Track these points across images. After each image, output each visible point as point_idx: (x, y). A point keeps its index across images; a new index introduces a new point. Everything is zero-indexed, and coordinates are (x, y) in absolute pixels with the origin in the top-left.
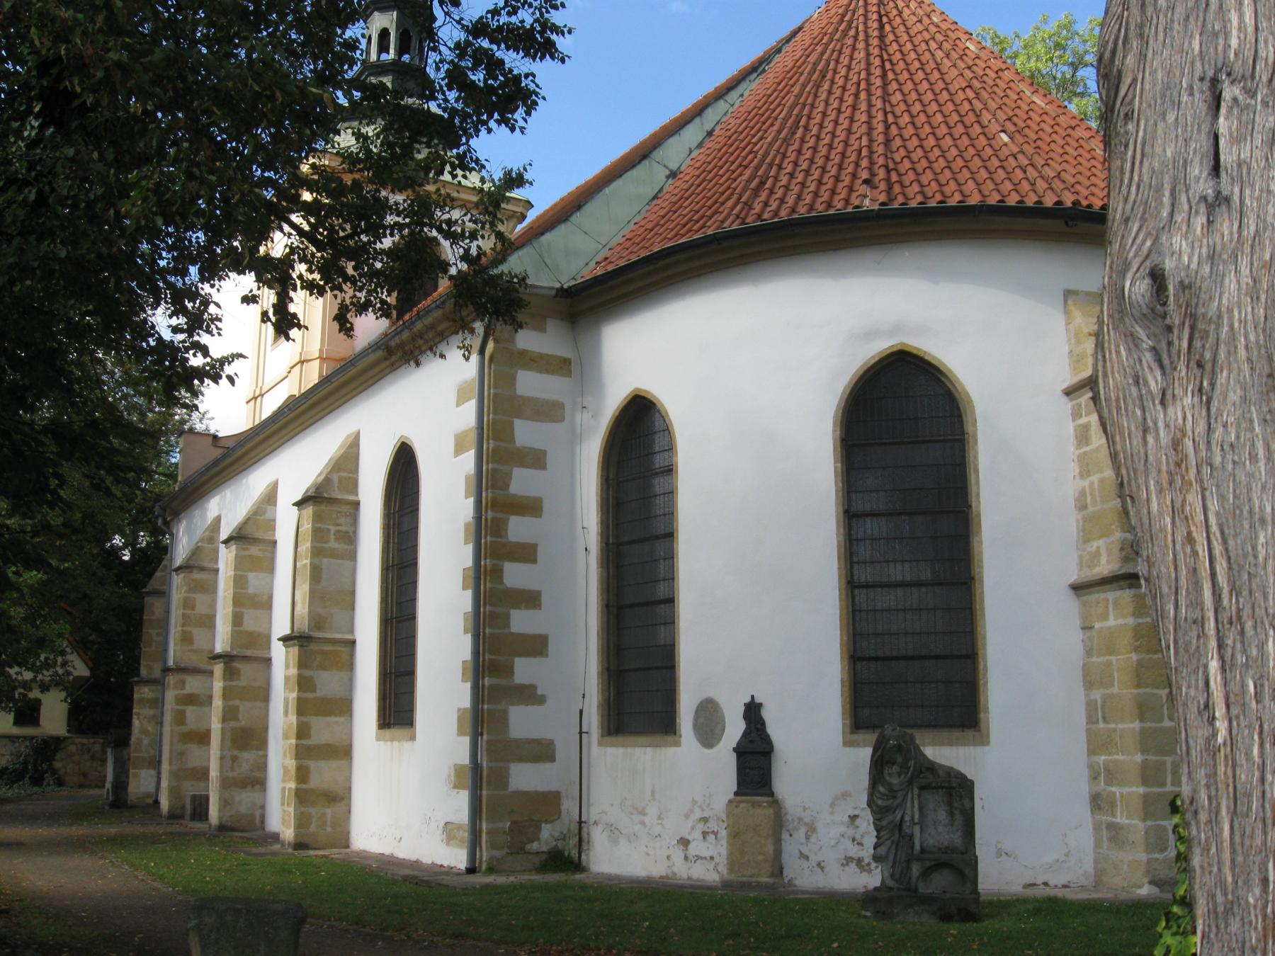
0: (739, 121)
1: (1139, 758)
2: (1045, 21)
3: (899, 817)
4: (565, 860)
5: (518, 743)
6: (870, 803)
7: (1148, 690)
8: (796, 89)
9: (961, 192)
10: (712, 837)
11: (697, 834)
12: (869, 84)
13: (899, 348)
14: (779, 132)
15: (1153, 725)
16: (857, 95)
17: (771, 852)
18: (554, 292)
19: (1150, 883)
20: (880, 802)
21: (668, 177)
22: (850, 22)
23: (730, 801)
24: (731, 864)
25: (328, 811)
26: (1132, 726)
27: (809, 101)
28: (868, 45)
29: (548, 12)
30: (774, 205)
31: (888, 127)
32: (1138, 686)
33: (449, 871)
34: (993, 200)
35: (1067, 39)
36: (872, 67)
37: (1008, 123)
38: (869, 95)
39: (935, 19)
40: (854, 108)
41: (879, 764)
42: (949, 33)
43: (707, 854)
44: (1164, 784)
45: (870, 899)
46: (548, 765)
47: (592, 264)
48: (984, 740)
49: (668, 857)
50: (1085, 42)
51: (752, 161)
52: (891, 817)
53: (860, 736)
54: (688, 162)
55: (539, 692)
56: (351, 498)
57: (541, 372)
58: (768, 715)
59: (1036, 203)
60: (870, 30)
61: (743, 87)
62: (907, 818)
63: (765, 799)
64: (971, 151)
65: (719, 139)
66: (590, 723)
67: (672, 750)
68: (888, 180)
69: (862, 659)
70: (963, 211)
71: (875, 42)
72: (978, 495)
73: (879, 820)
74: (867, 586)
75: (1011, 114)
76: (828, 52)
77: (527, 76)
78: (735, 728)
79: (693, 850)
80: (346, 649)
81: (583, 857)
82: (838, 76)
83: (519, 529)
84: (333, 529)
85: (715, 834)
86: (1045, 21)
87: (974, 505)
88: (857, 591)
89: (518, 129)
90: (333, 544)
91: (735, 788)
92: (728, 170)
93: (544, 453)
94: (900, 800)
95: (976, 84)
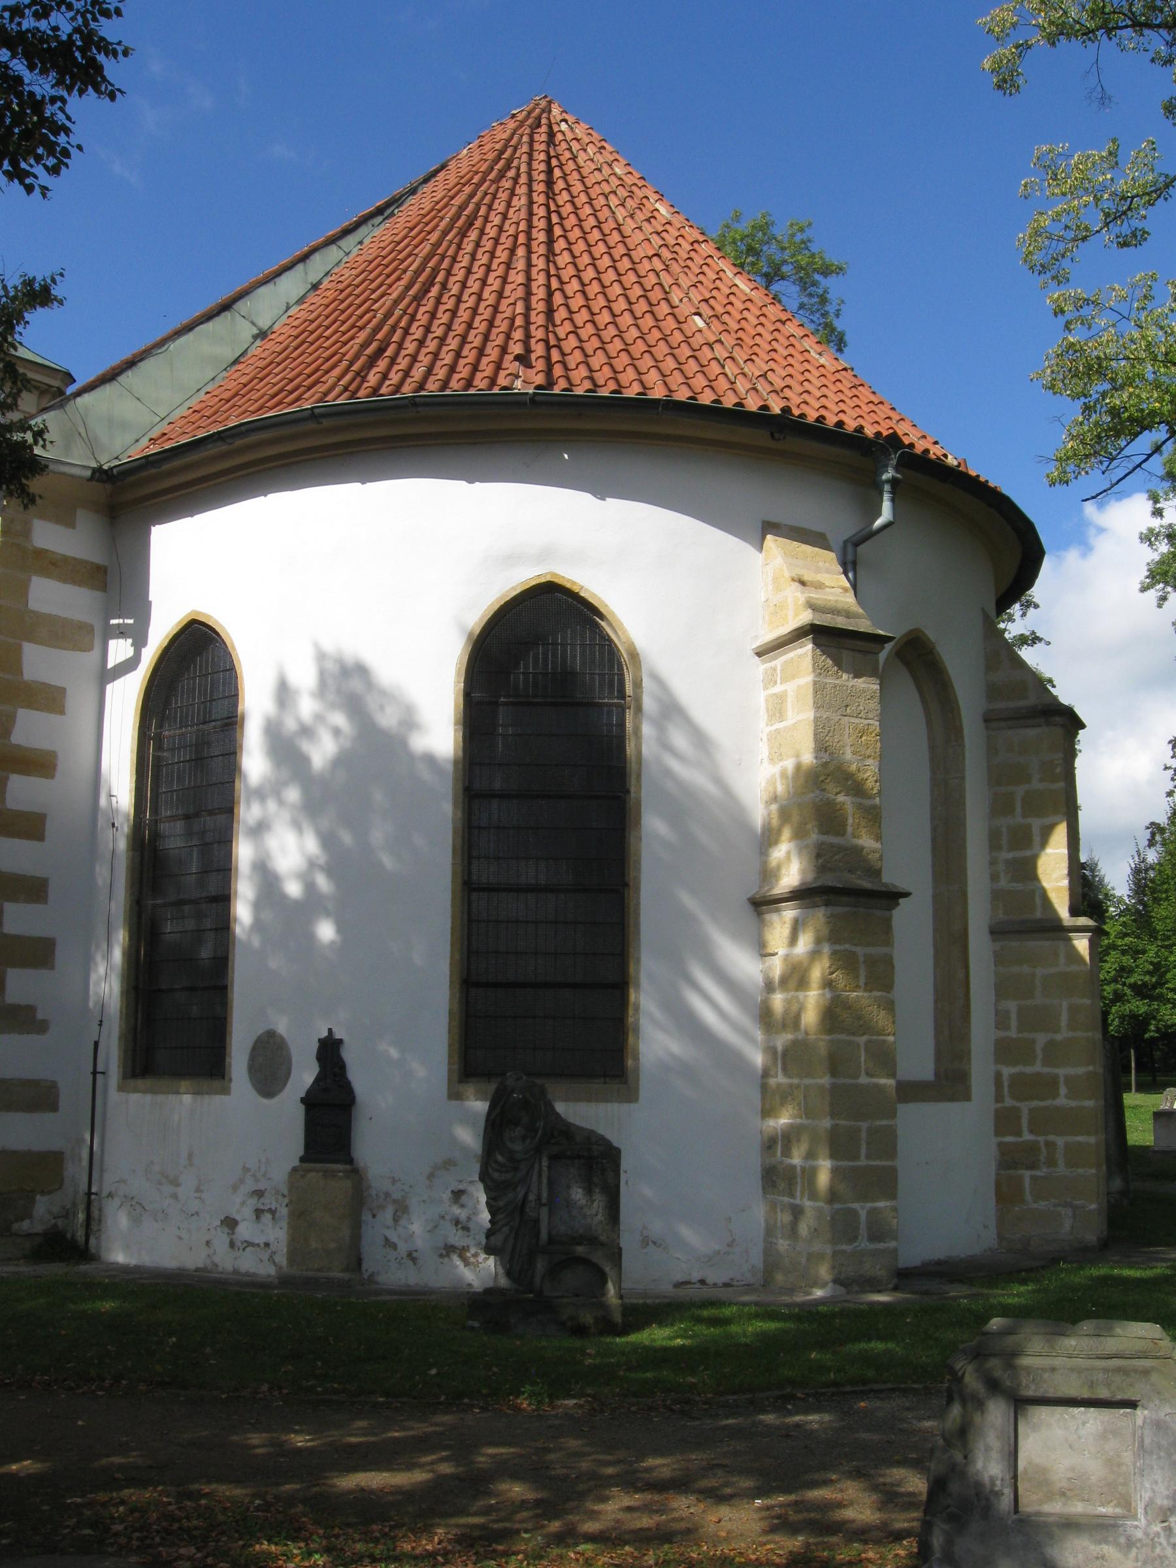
0: (354, 272)
1: (826, 1123)
2: (738, 218)
3: (521, 1196)
4: (69, 1245)
8: (433, 238)
9: (641, 382)
10: (269, 1216)
11: (248, 1212)
12: (530, 239)
13: (548, 578)
14: (408, 288)
16: (512, 251)
18: (88, 473)
20: (496, 1175)
21: (255, 337)
22: (509, 161)
23: (294, 1169)
24: (294, 1254)
27: (450, 252)
28: (531, 191)
29: (95, 20)
30: (394, 377)
31: (550, 294)
32: (830, 1031)
34: (682, 395)
35: (762, 243)
36: (535, 218)
37: (703, 305)
38: (529, 252)
39: (618, 171)
40: (508, 266)
41: (496, 1127)
42: (634, 188)
43: (260, 1240)
45: (481, 1304)
46: (48, 1117)
47: (145, 442)
49: (208, 1243)
50: (783, 249)
51: (369, 321)
53: (469, 1089)
54: (284, 320)
55: (40, 1016)
57: (65, 582)
58: (349, 1055)
59: (736, 404)
60: (535, 174)
61: (363, 230)
62: (532, 1197)
63: (340, 1167)
64: (656, 334)
65: (328, 293)
66: (107, 1064)
67: (218, 1099)
68: (548, 358)
69: (478, 985)
71: (541, 187)
73: (494, 1199)
74: (489, 889)
75: (708, 296)
76: (479, 194)
78: (305, 1074)
79: (245, 1230)
81: (92, 1241)
82: (489, 225)
85: (273, 1212)
86: (738, 218)
87: (633, 789)
88: (474, 895)
91: (301, 1152)
92: (336, 332)
93: (62, 691)
95: (665, 253)
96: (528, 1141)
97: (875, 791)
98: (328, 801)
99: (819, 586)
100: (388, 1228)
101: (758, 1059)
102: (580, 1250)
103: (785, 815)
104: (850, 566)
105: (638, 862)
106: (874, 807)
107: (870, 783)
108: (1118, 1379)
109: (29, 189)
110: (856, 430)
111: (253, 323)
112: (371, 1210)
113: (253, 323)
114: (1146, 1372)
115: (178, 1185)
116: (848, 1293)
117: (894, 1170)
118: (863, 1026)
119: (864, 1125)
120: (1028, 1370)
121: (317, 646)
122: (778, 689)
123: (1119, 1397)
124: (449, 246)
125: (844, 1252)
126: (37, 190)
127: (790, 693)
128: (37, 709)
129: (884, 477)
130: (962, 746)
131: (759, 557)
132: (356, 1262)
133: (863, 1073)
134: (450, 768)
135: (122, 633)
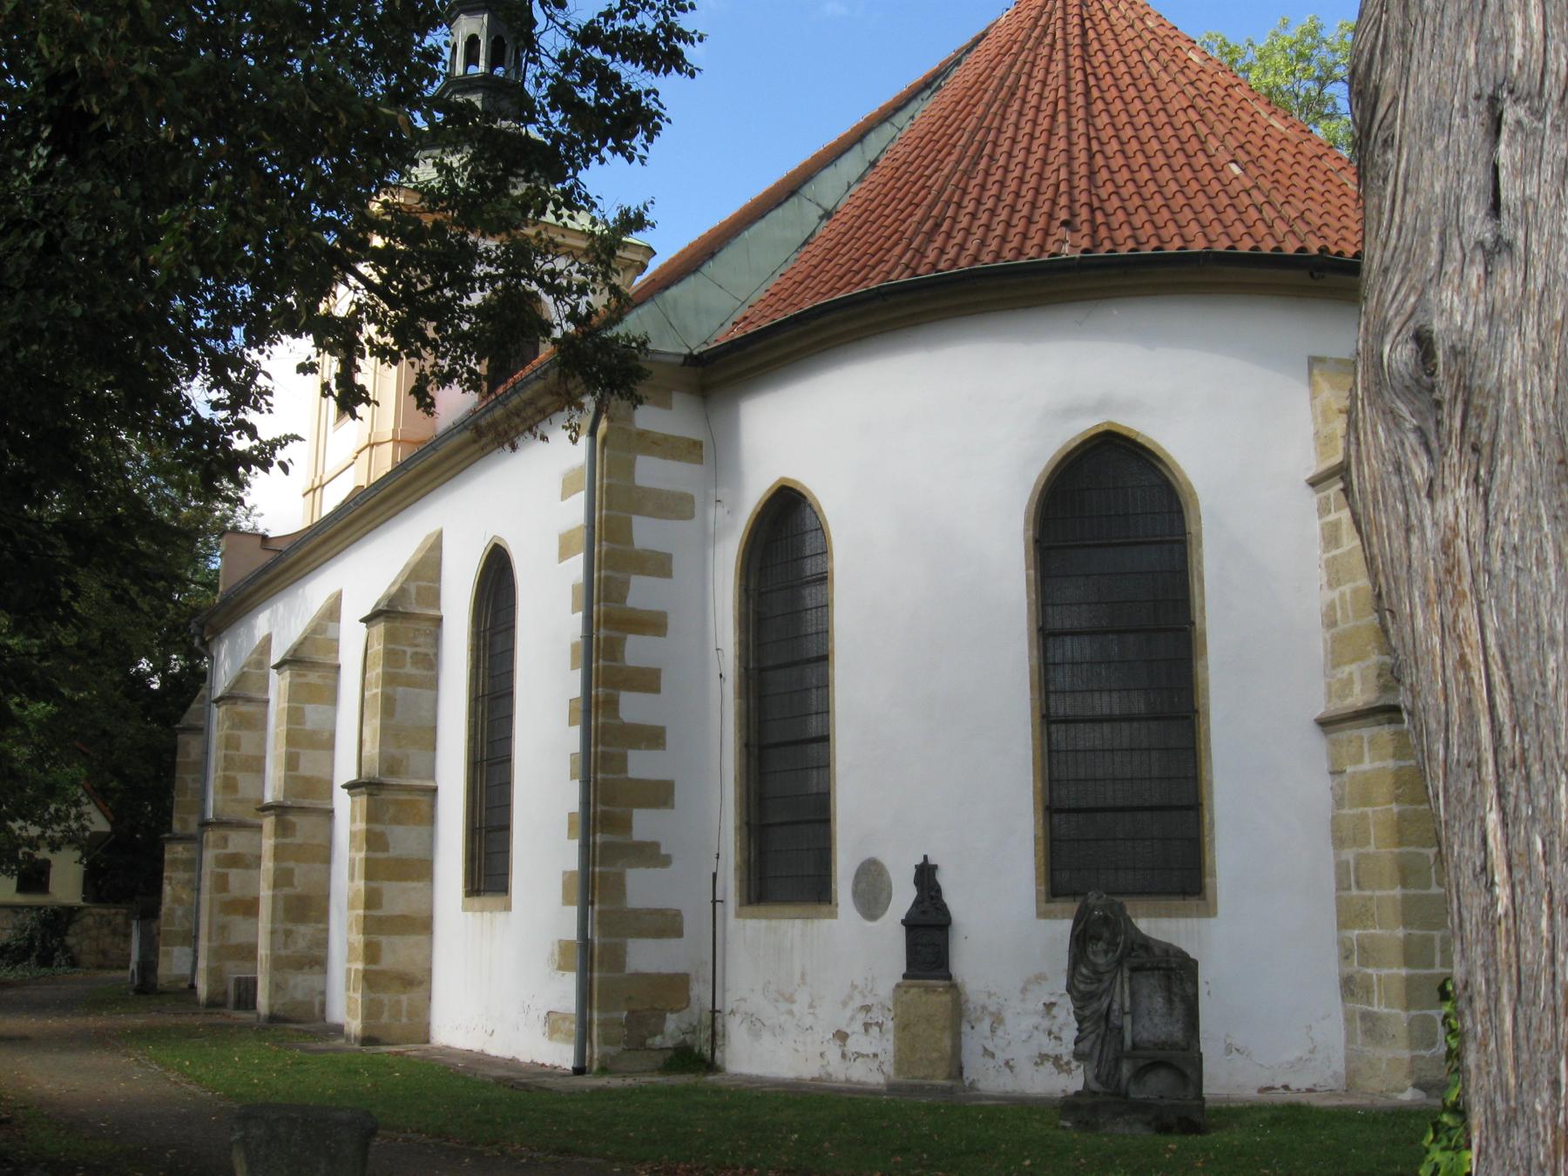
0: (909, 149)
1: (1400, 932)
2: (1285, 26)
3: (1105, 1005)
4: (695, 1058)
5: (637, 914)
6: (1070, 988)
7: (1412, 849)
8: (979, 110)
9: (1182, 236)
10: (875, 1029)
11: (857, 1026)
12: (1069, 103)
13: (1106, 428)
14: (958, 162)
15: (1418, 892)
16: (1053, 117)
17: (949, 1049)
18: (681, 360)
19: (1415, 1086)
20: (1082, 987)
21: (821, 218)
22: (1045, 28)
23: (898, 986)
24: (900, 1063)
25: (404, 998)
26: (1392, 893)
27: (995, 124)
28: (1067, 55)
29: (674, 15)
30: (952, 252)
31: (1091, 157)
32: (1400, 843)
33: (553, 1072)
34: (1221, 245)
35: (1312, 48)
36: (1073, 83)
37: (1239, 151)
38: (1069, 116)
39: (1150, 24)
40: (1051, 132)
41: (1081, 940)
42: (1167, 40)
43: (869, 1050)
44: (1431, 965)
45: (1070, 1106)
46: (673, 941)
47: (728, 325)
48: (1210, 911)
49: (822, 1055)
50: (1334, 51)
51: (925, 198)
52: (1095, 1005)
53: (1058, 906)
54: (846, 199)
55: (663, 851)
56: (432, 612)
57: (665, 458)
58: (944, 879)
59: (1275, 249)
60: (1070, 37)
61: (913, 107)
62: (1115, 1006)
63: (941, 983)
64: (1195, 186)
65: (885, 171)
66: (725, 890)
67: (827, 922)
68: (1092, 221)
69: (1061, 811)
70: (1184, 259)
71: (1076, 52)
72: (1203, 609)
73: (1081, 1008)
74: (1066, 721)
75: (1243, 140)
76: (1019, 64)
78: (904, 896)
79: (853, 1045)
80: (426, 799)
81: (718, 1054)
82: (1030, 94)
83: (638, 650)
84: (409, 650)
85: (880, 1025)
86: (1285, 26)
87: (1197, 621)
88: (1053, 727)
90: (409, 669)
91: (904, 970)
92: (895, 210)
93: (669, 557)
94: (1106, 984)
95: (1201, 104)
109: (630, 159)
126: (637, 159)
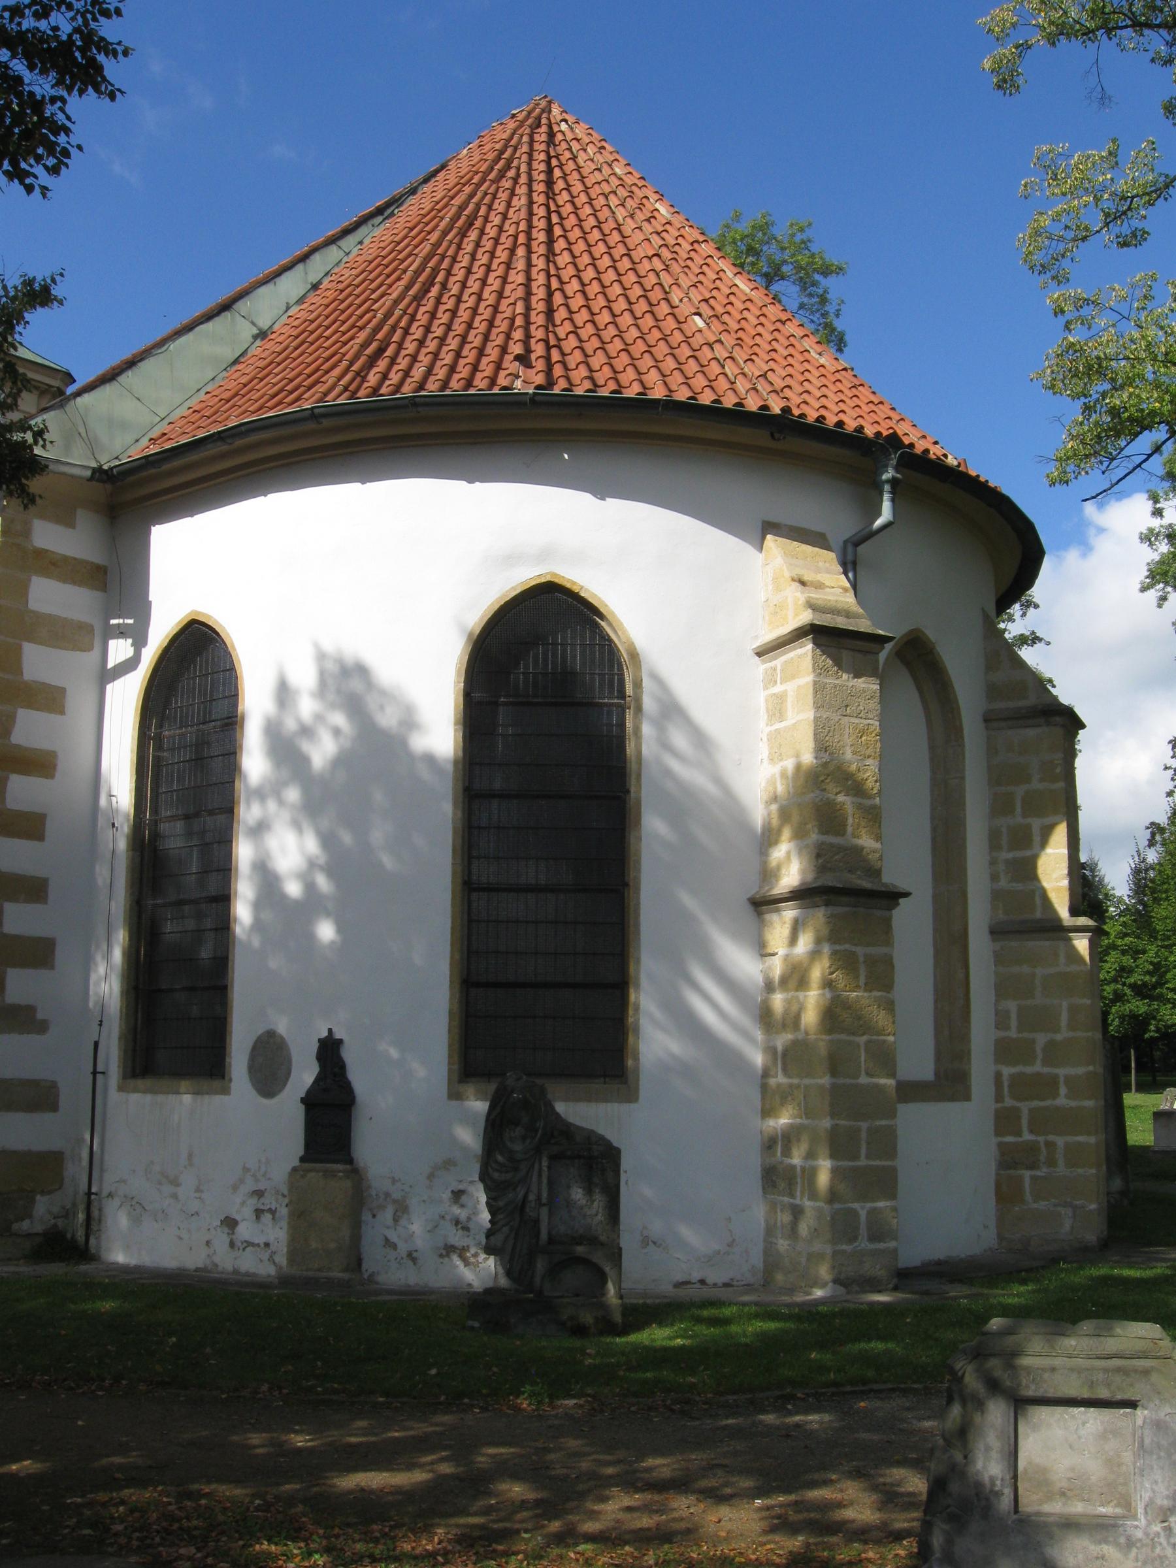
0: (354, 272)
1: (826, 1123)
2: (738, 218)
3: (521, 1196)
4: (69, 1245)
8: (433, 238)
9: (641, 382)
10: (269, 1216)
11: (248, 1212)
12: (530, 239)
13: (548, 578)
14: (408, 288)
16: (512, 251)
18: (88, 473)
20: (496, 1175)
21: (255, 337)
22: (509, 161)
23: (294, 1169)
24: (294, 1254)
27: (450, 252)
28: (531, 191)
29: (95, 20)
30: (394, 377)
31: (550, 294)
32: (830, 1031)
34: (682, 395)
35: (762, 243)
36: (535, 218)
37: (703, 305)
38: (529, 252)
39: (618, 171)
40: (508, 266)
41: (496, 1127)
42: (634, 188)
43: (260, 1240)
45: (481, 1304)
46: (48, 1117)
47: (145, 442)
49: (208, 1243)
50: (783, 249)
51: (369, 321)
53: (469, 1089)
54: (284, 320)
55: (40, 1016)
57: (65, 582)
58: (349, 1055)
59: (736, 404)
60: (535, 174)
61: (363, 230)
62: (532, 1197)
63: (340, 1167)
64: (656, 334)
65: (328, 293)
66: (107, 1064)
67: (218, 1099)
68: (548, 358)
69: (478, 985)
71: (541, 187)
73: (494, 1199)
74: (489, 889)
75: (708, 296)
76: (479, 194)
77: (53, 100)
78: (305, 1074)
79: (245, 1230)
81: (92, 1241)
82: (489, 225)
85: (273, 1212)
86: (738, 218)
87: (633, 789)
88: (474, 895)
89: (37, 190)
91: (301, 1152)
92: (336, 332)
93: (62, 691)
95: (665, 253)
96: (528, 1141)
97: (875, 791)
98: (328, 801)
99: (819, 586)
100: (388, 1228)
101: (758, 1059)
102: (580, 1250)
103: (785, 815)
104: (850, 566)
105: (638, 862)
106: (874, 807)
107: (870, 783)
108: (1118, 1379)
110: (856, 430)
111: (253, 323)
112: (371, 1210)
113: (253, 323)
114: (1146, 1372)
115: (178, 1185)
116: (848, 1293)
117: (894, 1170)
118: (863, 1026)
119: (864, 1125)
120: (1028, 1370)
121: (317, 646)
122: (778, 689)
123: (1119, 1397)
124: (449, 246)
125: (844, 1252)
127: (790, 693)
128: (37, 709)
129: (884, 477)
130: (962, 746)
131: (759, 557)
132: (356, 1262)
133: (863, 1073)
134: (450, 768)
135: (122, 633)
